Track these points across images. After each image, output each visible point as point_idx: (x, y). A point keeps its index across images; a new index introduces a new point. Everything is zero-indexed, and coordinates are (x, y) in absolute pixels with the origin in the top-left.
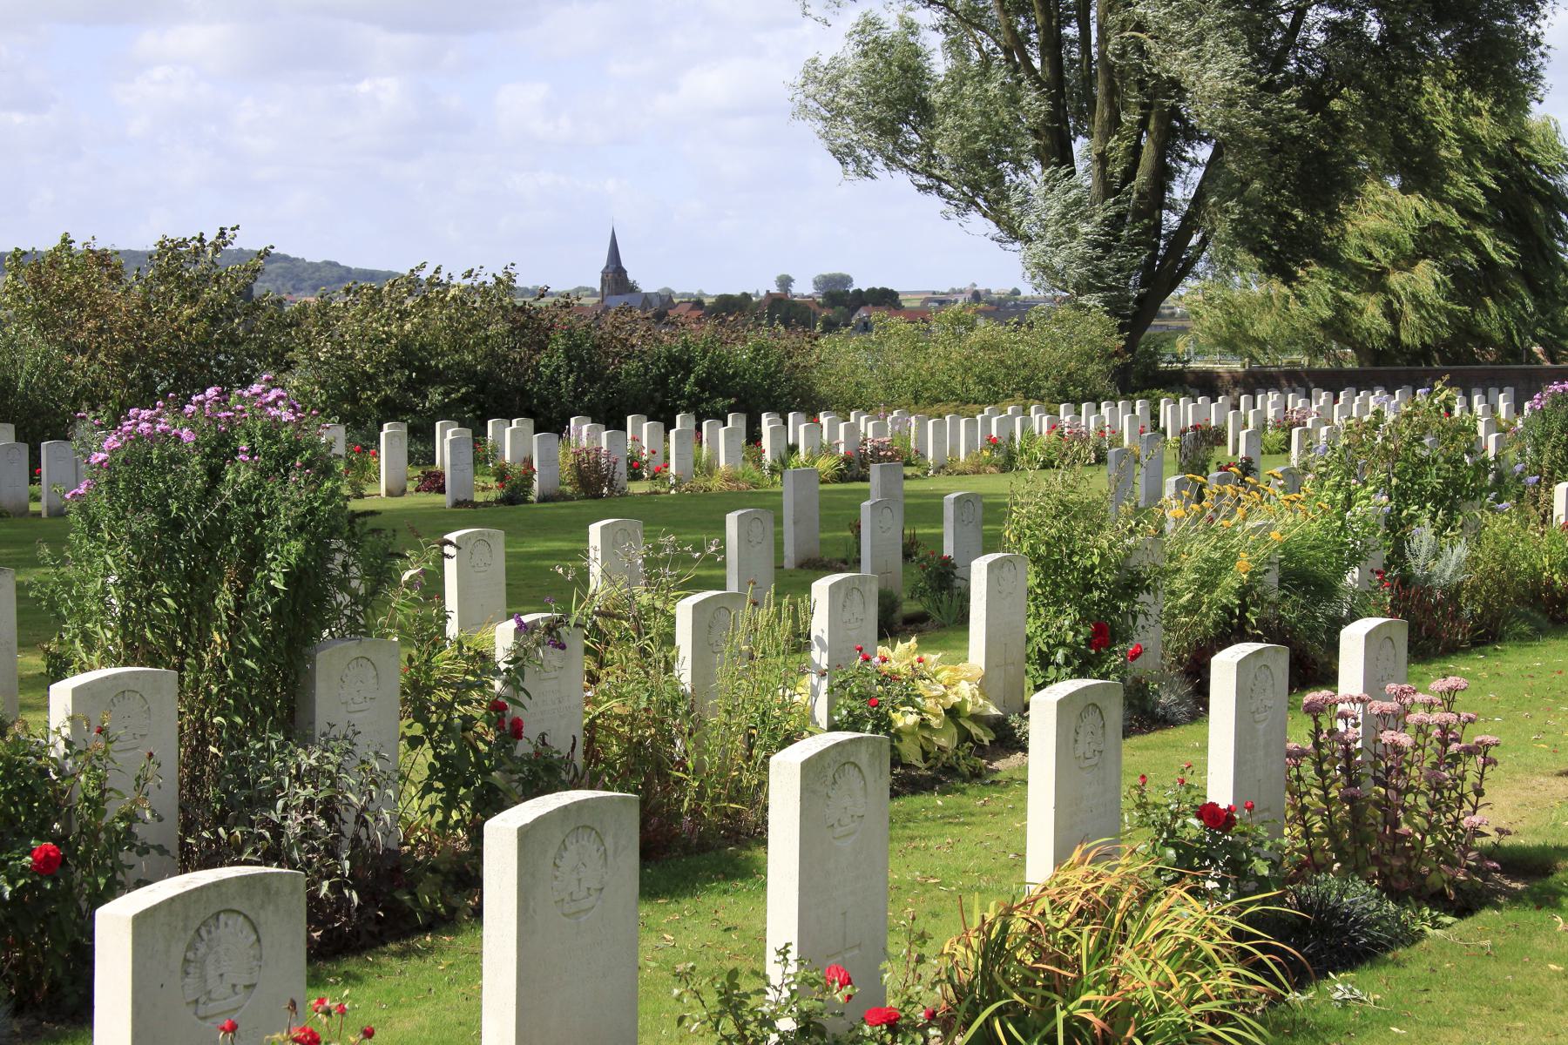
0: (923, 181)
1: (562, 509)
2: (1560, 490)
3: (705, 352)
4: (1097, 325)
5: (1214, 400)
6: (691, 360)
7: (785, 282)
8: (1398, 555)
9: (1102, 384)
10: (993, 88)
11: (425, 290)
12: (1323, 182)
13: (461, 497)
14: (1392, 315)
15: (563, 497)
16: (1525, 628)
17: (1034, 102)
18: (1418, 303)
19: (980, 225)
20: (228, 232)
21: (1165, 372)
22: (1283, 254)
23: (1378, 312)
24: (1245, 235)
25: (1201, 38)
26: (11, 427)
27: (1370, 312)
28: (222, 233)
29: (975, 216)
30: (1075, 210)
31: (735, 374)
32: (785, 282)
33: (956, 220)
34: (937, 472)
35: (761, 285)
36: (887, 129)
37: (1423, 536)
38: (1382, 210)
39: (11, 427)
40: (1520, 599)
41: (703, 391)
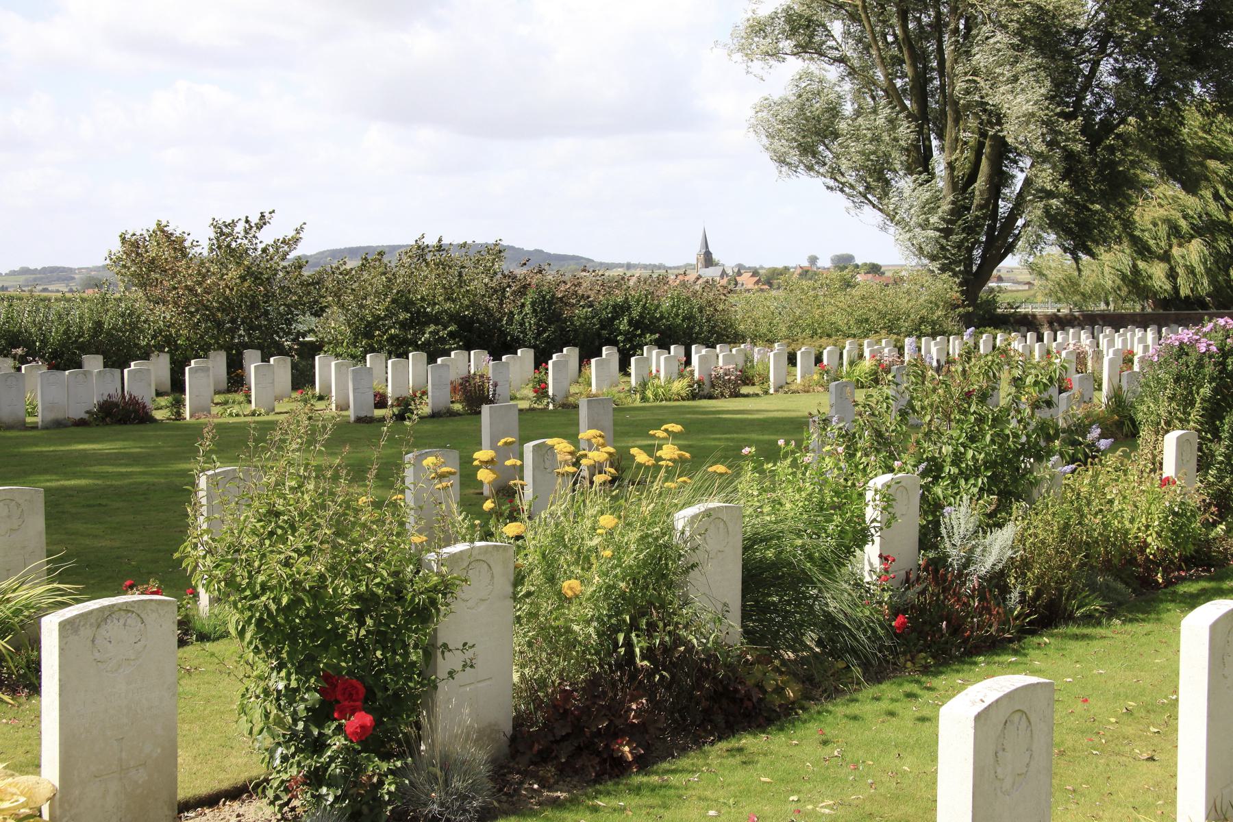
0: (832, 183)
1: (450, 425)
2: (269, 811)
3: (638, 301)
4: (948, 286)
5: (1117, 331)
6: (629, 307)
7: (813, 260)
8: (929, 536)
9: (949, 325)
10: (881, 121)
11: (585, 265)
12: (1119, 187)
13: (363, 414)
14: (1172, 275)
15: (451, 414)
16: (1096, 606)
17: (905, 131)
18: (1191, 270)
19: (871, 216)
20: (267, 215)
21: (1003, 315)
22: (1080, 234)
23: (1162, 276)
24: (1054, 221)
25: (1015, 79)
26: (100, 358)
27: (1157, 273)
28: (263, 216)
29: (868, 209)
30: (930, 206)
31: (662, 317)
32: (813, 260)
33: (852, 212)
34: (776, 391)
35: (797, 260)
36: (807, 150)
37: (960, 517)
38: (1160, 203)
39: (100, 358)
40: (1108, 566)
41: (636, 329)
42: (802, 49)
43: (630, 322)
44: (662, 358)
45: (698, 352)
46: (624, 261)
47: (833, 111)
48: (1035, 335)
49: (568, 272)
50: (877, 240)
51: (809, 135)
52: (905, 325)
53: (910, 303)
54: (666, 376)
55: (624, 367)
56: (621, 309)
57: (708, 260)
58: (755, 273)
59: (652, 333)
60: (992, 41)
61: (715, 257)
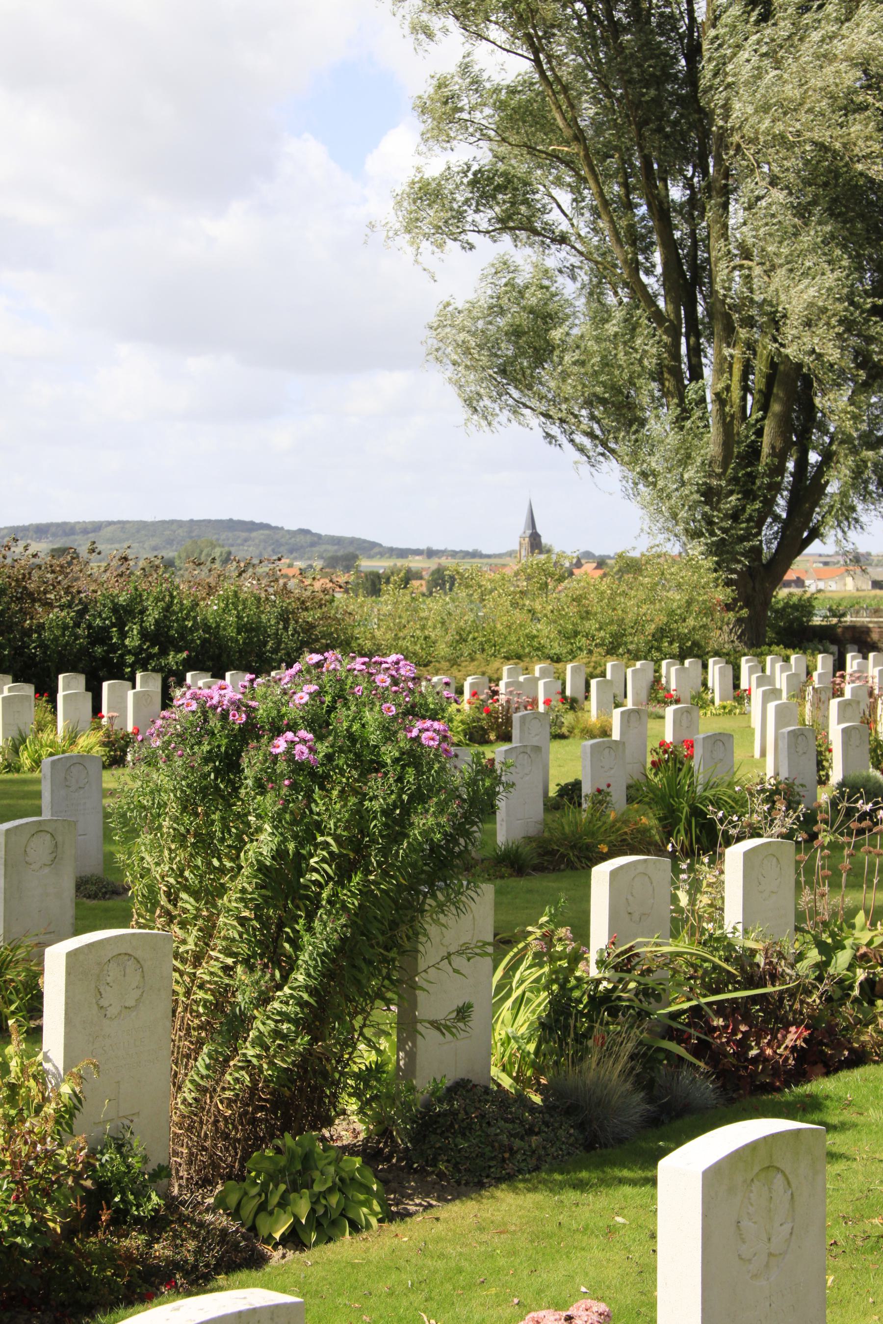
42: (505, 224)
43: (144, 635)
44: (673, 670)
45: (852, 661)
46: (423, 546)
47: (546, 316)
48: (830, 660)
49: (142, 554)
50: (607, 513)
51: (515, 352)
52: (636, 641)
53: (642, 609)
54: (66, 728)
55: (167, 701)
56: (123, 614)
57: (535, 542)
58: (601, 563)
59: (179, 650)
60: (763, 203)
61: (544, 540)
